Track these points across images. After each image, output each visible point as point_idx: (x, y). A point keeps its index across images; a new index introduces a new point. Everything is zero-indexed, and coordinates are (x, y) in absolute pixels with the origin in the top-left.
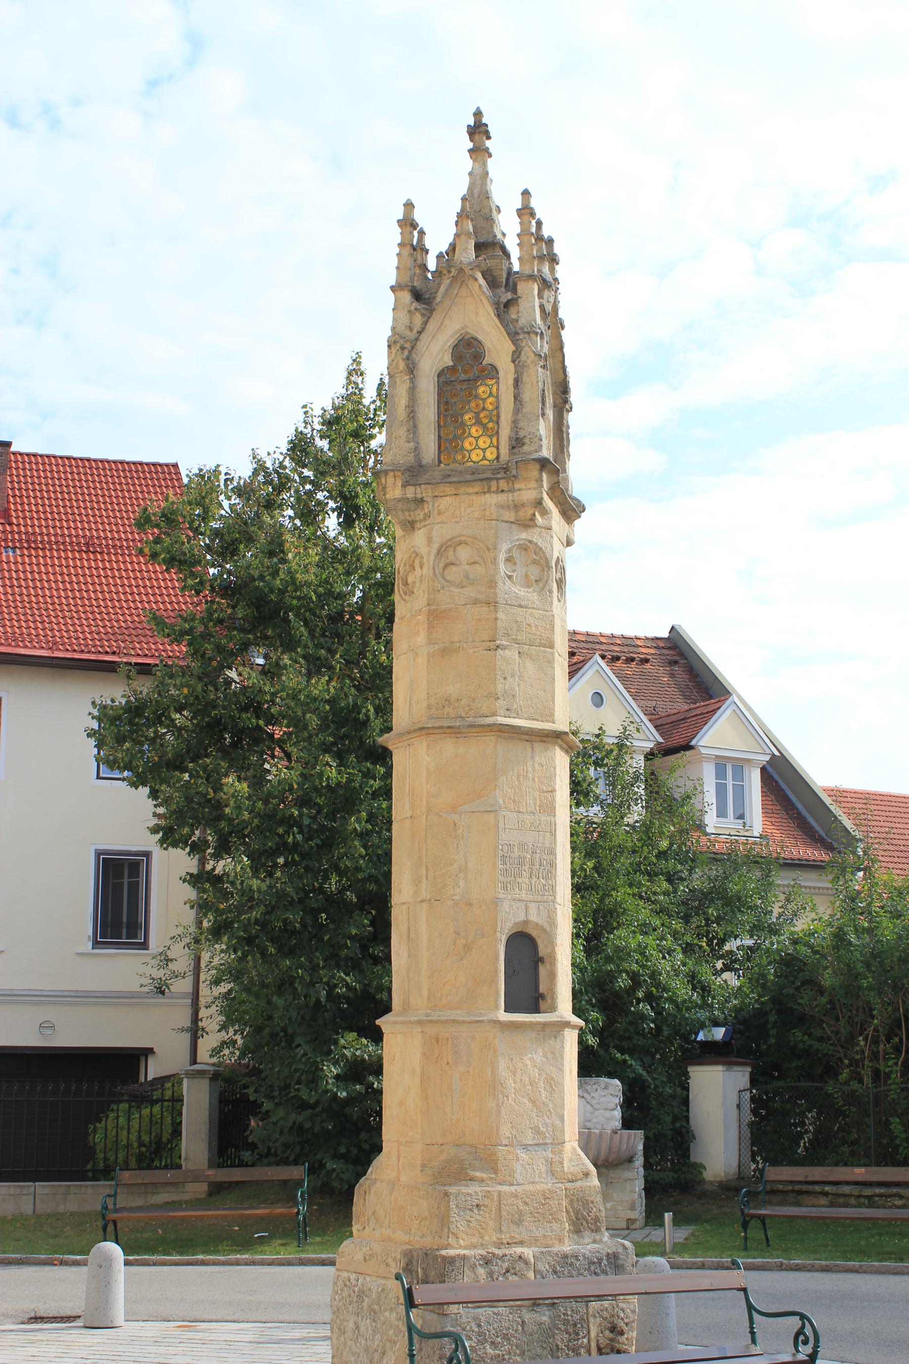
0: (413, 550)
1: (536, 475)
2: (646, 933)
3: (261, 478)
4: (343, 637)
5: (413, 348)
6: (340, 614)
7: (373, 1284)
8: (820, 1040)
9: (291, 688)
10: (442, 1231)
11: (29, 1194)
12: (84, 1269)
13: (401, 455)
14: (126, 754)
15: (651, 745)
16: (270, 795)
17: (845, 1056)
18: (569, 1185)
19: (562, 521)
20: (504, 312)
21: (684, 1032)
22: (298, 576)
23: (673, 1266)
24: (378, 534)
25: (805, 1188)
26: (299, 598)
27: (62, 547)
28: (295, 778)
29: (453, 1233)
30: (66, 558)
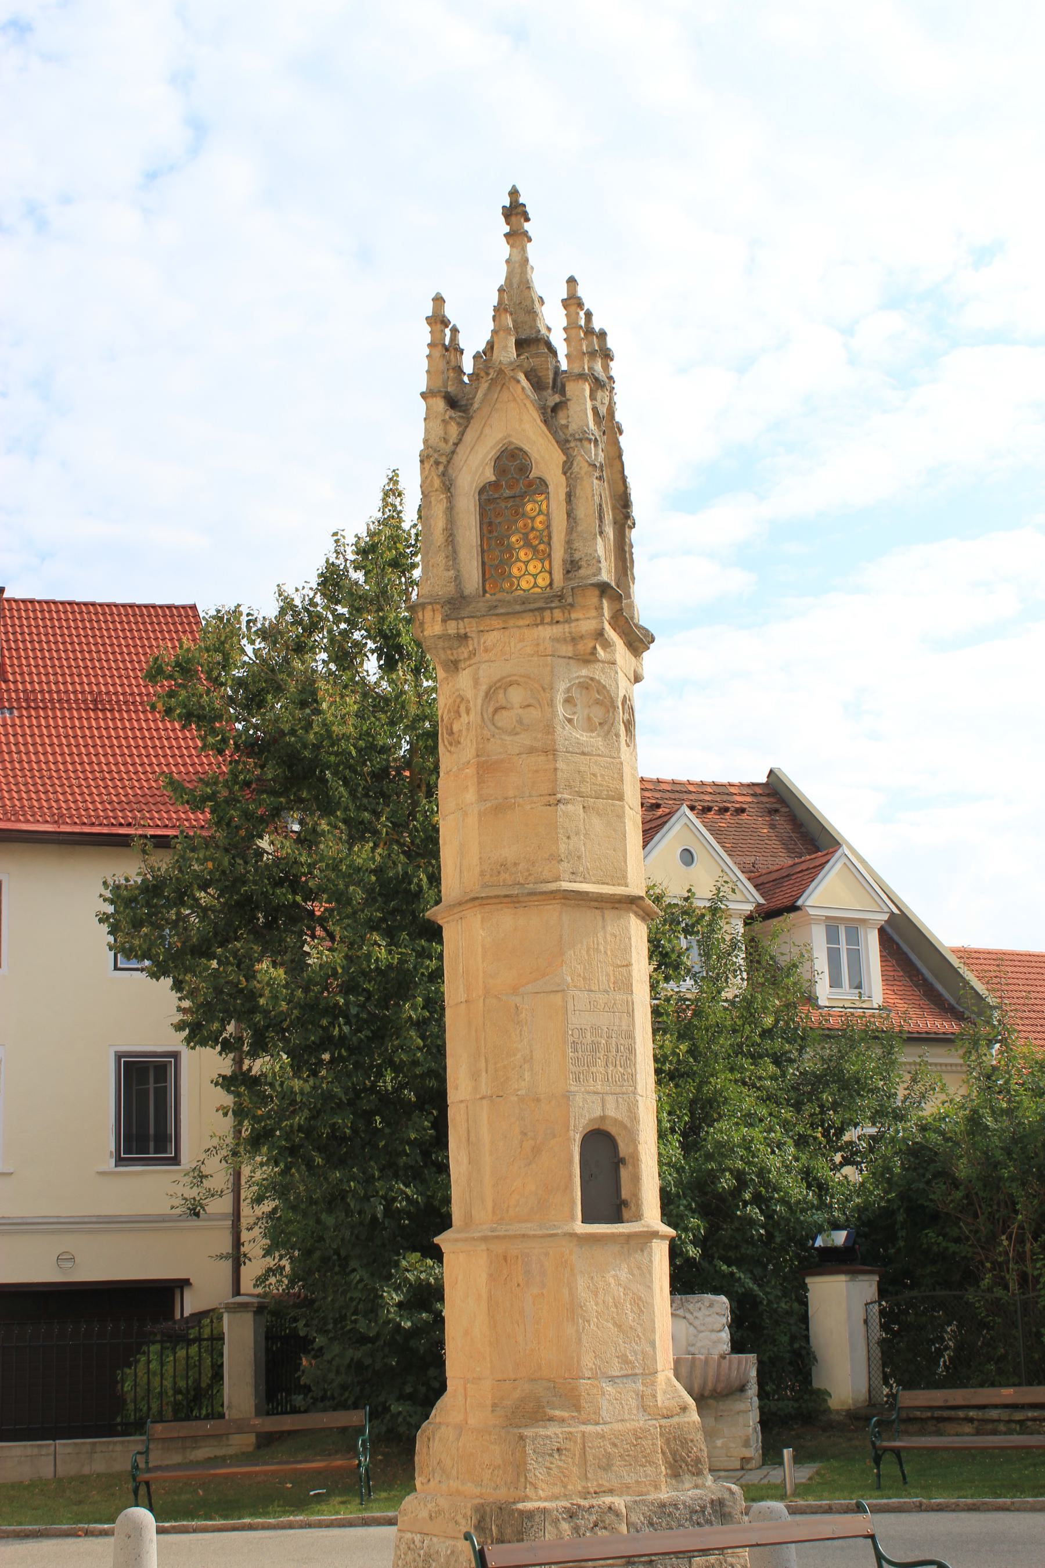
0: (454, 692)
1: (597, 604)
2: (751, 1125)
3: (289, 618)
4: (389, 797)
5: (449, 462)
6: (385, 771)
7: (442, 1546)
8: (957, 1240)
9: (330, 858)
10: (518, 1481)
11: (48, 1455)
12: (110, 1540)
13: (441, 585)
14: (144, 941)
15: (750, 907)
16: (310, 981)
17: (987, 1258)
18: (664, 1422)
19: (628, 654)
20: (552, 417)
21: (801, 1236)
22: (334, 728)
23: (793, 1511)
24: (425, 677)
25: (946, 1414)
26: (337, 754)
27: (65, 705)
28: (339, 961)
29: (531, 1483)
30: (38, 717)
